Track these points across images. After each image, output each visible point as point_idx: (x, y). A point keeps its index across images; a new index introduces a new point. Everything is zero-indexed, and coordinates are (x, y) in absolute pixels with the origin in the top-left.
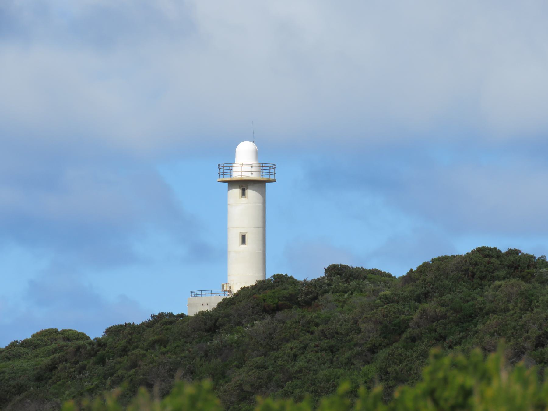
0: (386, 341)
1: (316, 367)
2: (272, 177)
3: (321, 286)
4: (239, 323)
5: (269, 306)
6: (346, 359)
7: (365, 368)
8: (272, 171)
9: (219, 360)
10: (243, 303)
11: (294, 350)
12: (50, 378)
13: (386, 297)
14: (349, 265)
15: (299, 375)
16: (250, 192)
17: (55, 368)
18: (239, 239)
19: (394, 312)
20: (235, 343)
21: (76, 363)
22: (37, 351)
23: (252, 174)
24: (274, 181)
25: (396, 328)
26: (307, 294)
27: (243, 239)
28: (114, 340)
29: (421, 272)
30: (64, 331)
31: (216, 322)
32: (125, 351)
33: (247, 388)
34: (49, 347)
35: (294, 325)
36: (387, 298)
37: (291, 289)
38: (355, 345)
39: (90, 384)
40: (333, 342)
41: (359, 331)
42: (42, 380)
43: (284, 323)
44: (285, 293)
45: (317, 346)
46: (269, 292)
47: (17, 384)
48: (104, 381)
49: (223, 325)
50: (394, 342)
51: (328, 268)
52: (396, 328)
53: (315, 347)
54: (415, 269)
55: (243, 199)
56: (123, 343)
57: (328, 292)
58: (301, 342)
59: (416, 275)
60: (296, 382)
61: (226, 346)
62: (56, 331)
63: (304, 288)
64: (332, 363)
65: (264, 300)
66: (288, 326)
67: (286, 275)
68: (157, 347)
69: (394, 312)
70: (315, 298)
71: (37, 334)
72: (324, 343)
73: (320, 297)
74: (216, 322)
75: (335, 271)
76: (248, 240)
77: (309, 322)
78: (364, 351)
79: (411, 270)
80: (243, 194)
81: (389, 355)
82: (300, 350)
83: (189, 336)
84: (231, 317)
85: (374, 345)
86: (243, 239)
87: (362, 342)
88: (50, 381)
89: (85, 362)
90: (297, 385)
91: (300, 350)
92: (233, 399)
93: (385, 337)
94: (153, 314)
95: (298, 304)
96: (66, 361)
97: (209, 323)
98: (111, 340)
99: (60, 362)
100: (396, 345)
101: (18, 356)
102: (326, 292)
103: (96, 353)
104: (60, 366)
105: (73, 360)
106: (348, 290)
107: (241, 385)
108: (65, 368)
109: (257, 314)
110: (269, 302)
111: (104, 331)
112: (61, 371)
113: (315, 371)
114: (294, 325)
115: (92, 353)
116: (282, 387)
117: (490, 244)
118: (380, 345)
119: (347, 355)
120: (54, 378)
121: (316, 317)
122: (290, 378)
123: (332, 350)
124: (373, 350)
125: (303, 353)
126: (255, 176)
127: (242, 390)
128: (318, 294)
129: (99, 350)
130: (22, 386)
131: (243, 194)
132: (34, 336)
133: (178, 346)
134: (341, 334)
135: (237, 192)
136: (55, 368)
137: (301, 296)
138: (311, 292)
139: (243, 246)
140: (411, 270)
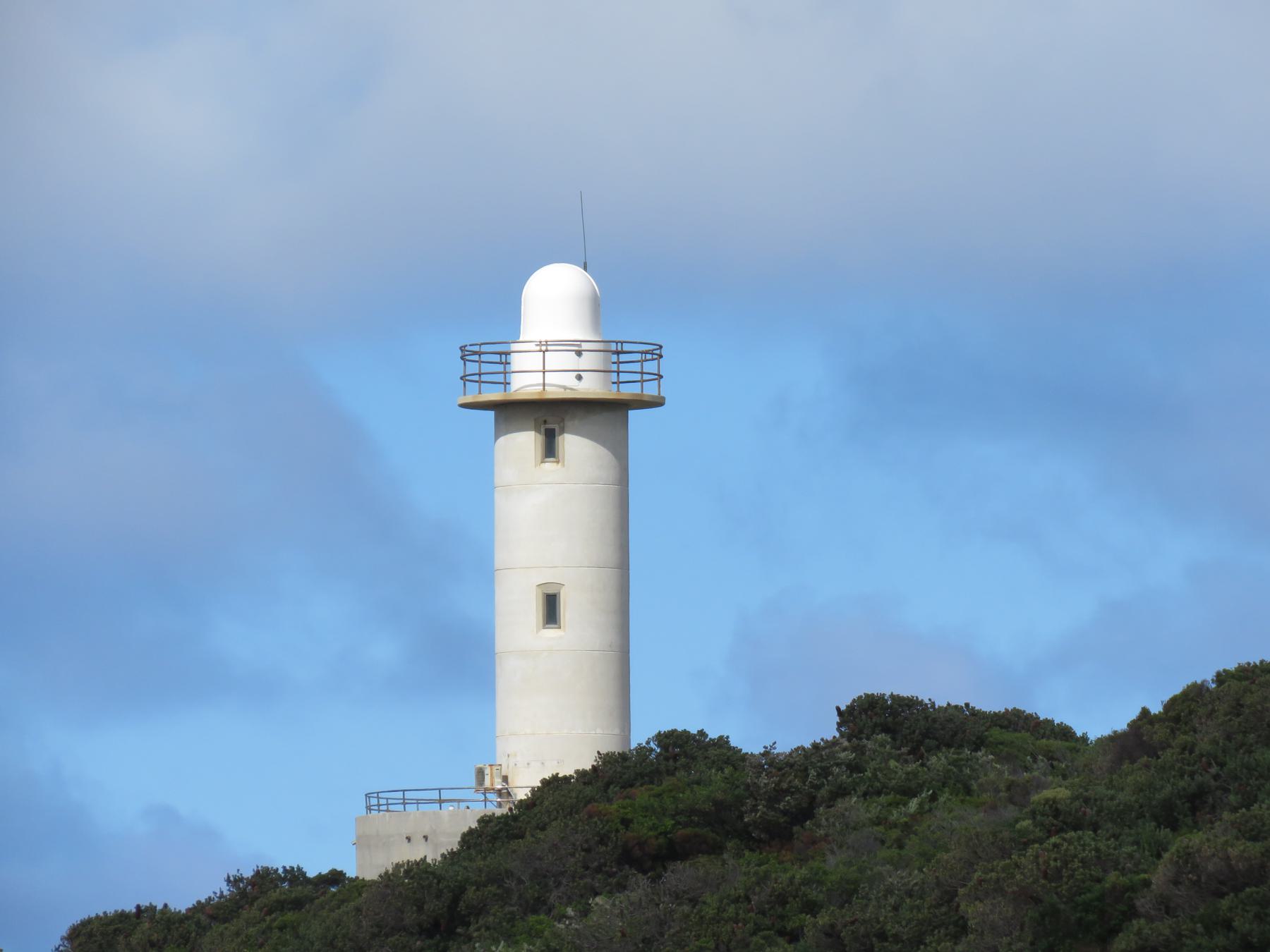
2: (650, 390)
4: (538, 905)
8: (651, 367)
13: (1054, 808)
14: (924, 697)
16: (576, 446)
23: (579, 378)
24: (657, 403)
25: (1091, 917)
26: (779, 793)
27: (551, 609)
31: (456, 900)
36: (1057, 813)
37: (716, 785)
43: (694, 902)
51: (851, 708)
52: (1091, 917)
54: (1156, 708)
55: (549, 466)
59: (1160, 733)
65: (626, 822)
66: (710, 912)
70: (805, 813)
74: (456, 900)
76: (566, 610)
77: (782, 899)
79: (1145, 712)
80: (550, 451)
84: (510, 884)
86: (551, 609)
94: (233, 873)
102: (842, 792)
106: (921, 787)
109: (599, 870)
114: (731, 909)
121: (806, 882)
126: (591, 387)
131: (550, 451)
135: (526, 441)
137: (754, 809)
139: (551, 633)
140: (1145, 712)
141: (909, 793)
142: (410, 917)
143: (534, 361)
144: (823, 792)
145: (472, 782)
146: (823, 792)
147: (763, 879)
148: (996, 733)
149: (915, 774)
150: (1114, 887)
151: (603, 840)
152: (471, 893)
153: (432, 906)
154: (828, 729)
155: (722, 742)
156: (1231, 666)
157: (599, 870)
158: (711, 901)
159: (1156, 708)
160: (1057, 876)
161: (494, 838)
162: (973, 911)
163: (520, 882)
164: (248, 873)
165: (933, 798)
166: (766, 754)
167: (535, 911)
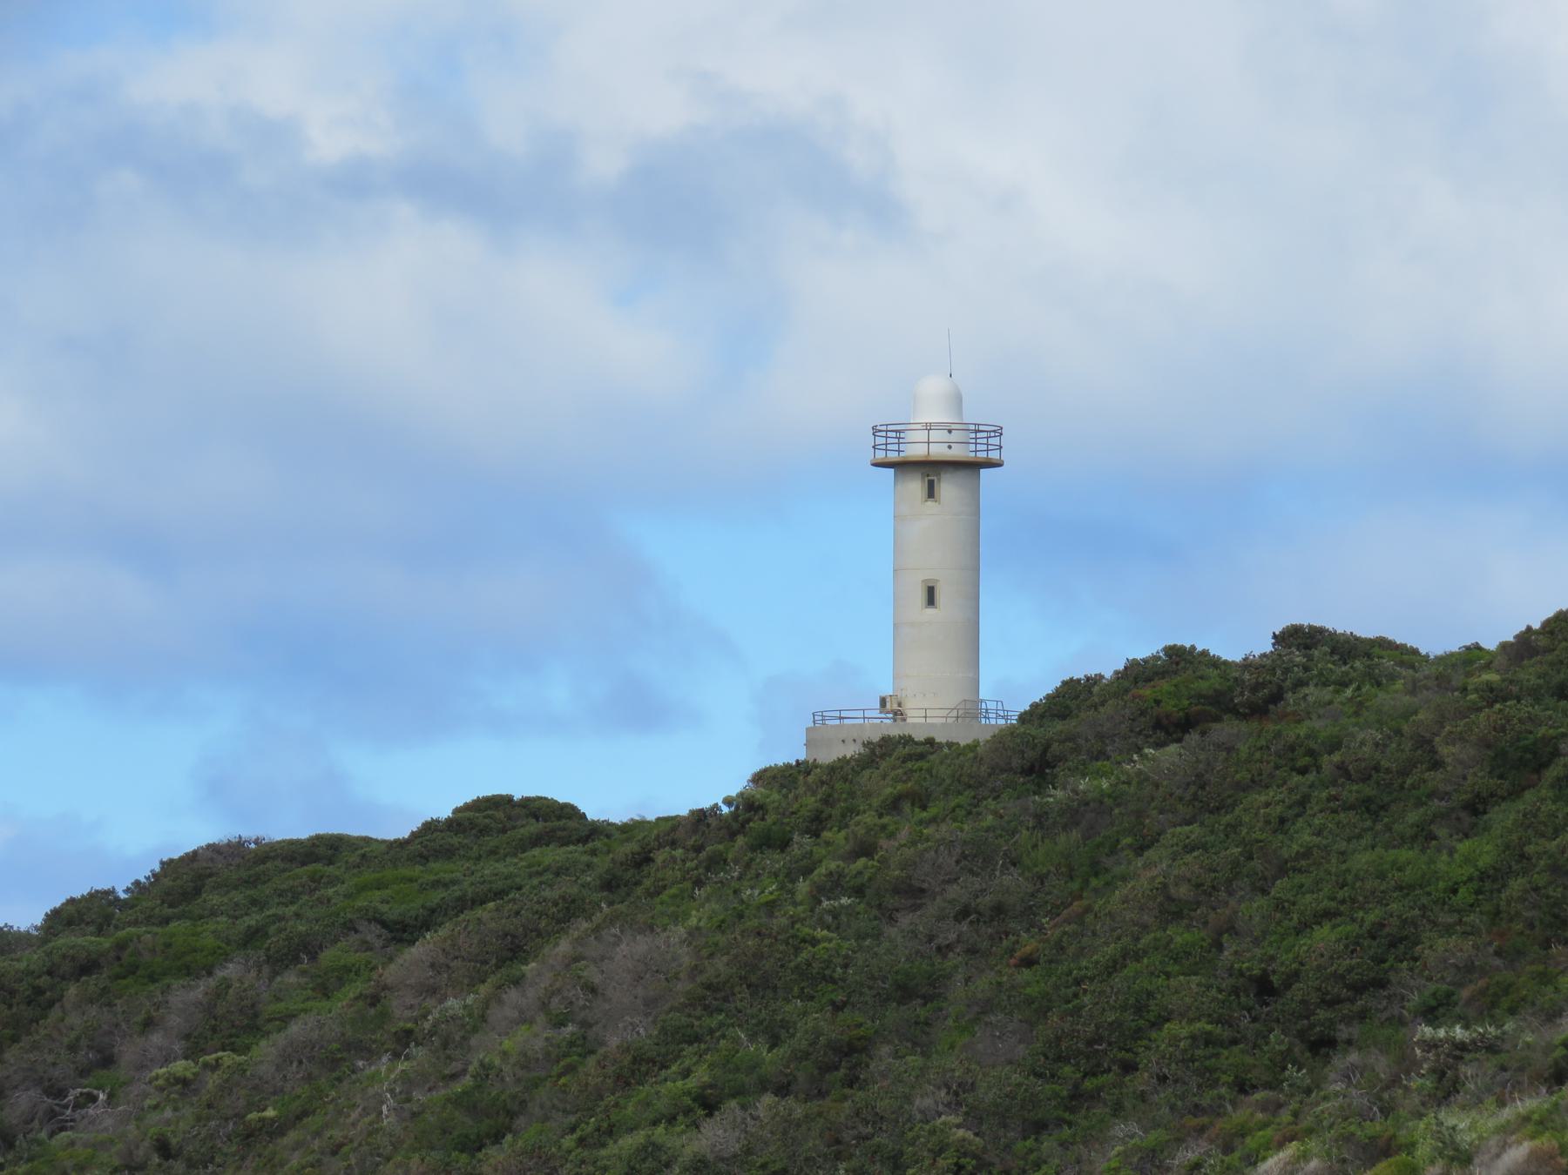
0: (1506, 784)
1: (1343, 845)
2: (994, 455)
3: (1287, 671)
4: (1101, 755)
5: (1168, 716)
6: (1412, 826)
7: (1464, 847)
8: (995, 441)
9: (1075, 834)
10: (1107, 710)
11: (1279, 809)
12: (638, 883)
13: (1490, 688)
14: (1329, 626)
15: (1303, 863)
16: (949, 488)
17: (649, 860)
18: (920, 596)
19: (1520, 720)
20: (1110, 796)
21: (698, 849)
22: (491, 841)
24: (998, 464)
25: (1529, 756)
26: (1255, 688)
27: (931, 597)
28: (786, 796)
29: (1552, 633)
30: (527, 800)
31: (1045, 751)
32: (816, 824)
33: (1183, 891)
34: (522, 830)
35: (1258, 755)
36: (1492, 690)
37: (1213, 682)
38: (1431, 796)
39: (757, 892)
40: (1368, 790)
41: (1437, 764)
42: (618, 886)
43: (1229, 750)
44: (1203, 686)
45: (1335, 798)
46: (1165, 685)
47: (563, 898)
48: (790, 886)
49: (1061, 758)
50: (1523, 790)
51: (1283, 633)
52: (1529, 756)
53: (1328, 800)
54: (1536, 626)
55: (930, 503)
56: (811, 802)
57: (1307, 684)
58: (1291, 790)
59: (1543, 642)
60: (1299, 879)
61: (1087, 804)
62: (508, 800)
63: (1247, 676)
64: (603, 958)
65: (1158, 702)
66: (1243, 756)
67: (1193, 647)
68: (906, 807)
69: (1520, 720)
70: (1277, 697)
71: (467, 807)
72: (1351, 792)
73: (1289, 696)
74: (1045, 751)
75: (1297, 639)
76: (940, 597)
77: (1292, 749)
78: (1453, 809)
79: (1529, 629)
80: (931, 493)
81: (1525, 815)
82: (1290, 807)
83: (981, 784)
84: (1081, 741)
85: (1478, 795)
86: (931, 597)
87: (1449, 788)
88: (639, 891)
89: (721, 847)
90: (1302, 886)
91: (1290, 807)
92: (1146, 918)
93: (1501, 777)
95: (1234, 711)
96: (673, 844)
97: (1030, 754)
98: (776, 796)
99: (660, 846)
100: (1529, 796)
101: (448, 853)
102: (1301, 683)
103: (743, 826)
104: (660, 856)
105: (690, 842)
106: (1351, 682)
107: (1165, 886)
108: (674, 859)
109: (1140, 733)
110: (1169, 706)
111: (749, 777)
112: (664, 867)
113: (1343, 853)
114: (1258, 755)
115: (735, 826)
116: (1265, 892)
117: (523, 778)
118: (1492, 795)
119: (1413, 816)
120: (647, 883)
121: (1308, 737)
122: (1283, 870)
123: (1371, 808)
124: (1477, 806)
125: (1298, 815)
126: (958, 453)
127: (1170, 899)
128: (1280, 688)
129: (749, 820)
130: (573, 901)
131: (931, 493)
132: (457, 811)
133: (959, 806)
134: (1388, 771)
135: (916, 486)
136: (649, 860)
137: (1242, 694)
138: (1264, 685)
139: (931, 611)
140: (1529, 629)
141: (1346, 685)
142: (1016, 762)
143: (922, 436)
144: (1288, 683)
145: (878, 706)
146: (1288, 683)
147: (1278, 735)
148: (1376, 650)
149: (1347, 673)
150: (1544, 737)
151: (1143, 713)
152: (1055, 746)
153: (1030, 754)
154: (1267, 646)
155: (1205, 653)
156: (460, 804)
157: (1140, 733)
158: (1244, 749)
159: (1536, 626)
160: (1503, 729)
161: (1042, 717)
162: (1445, 751)
163: (1087, 740)
164: (876, 738)
165: (1359, 688)
166: (1245, 659)
167: (1097, 759)
